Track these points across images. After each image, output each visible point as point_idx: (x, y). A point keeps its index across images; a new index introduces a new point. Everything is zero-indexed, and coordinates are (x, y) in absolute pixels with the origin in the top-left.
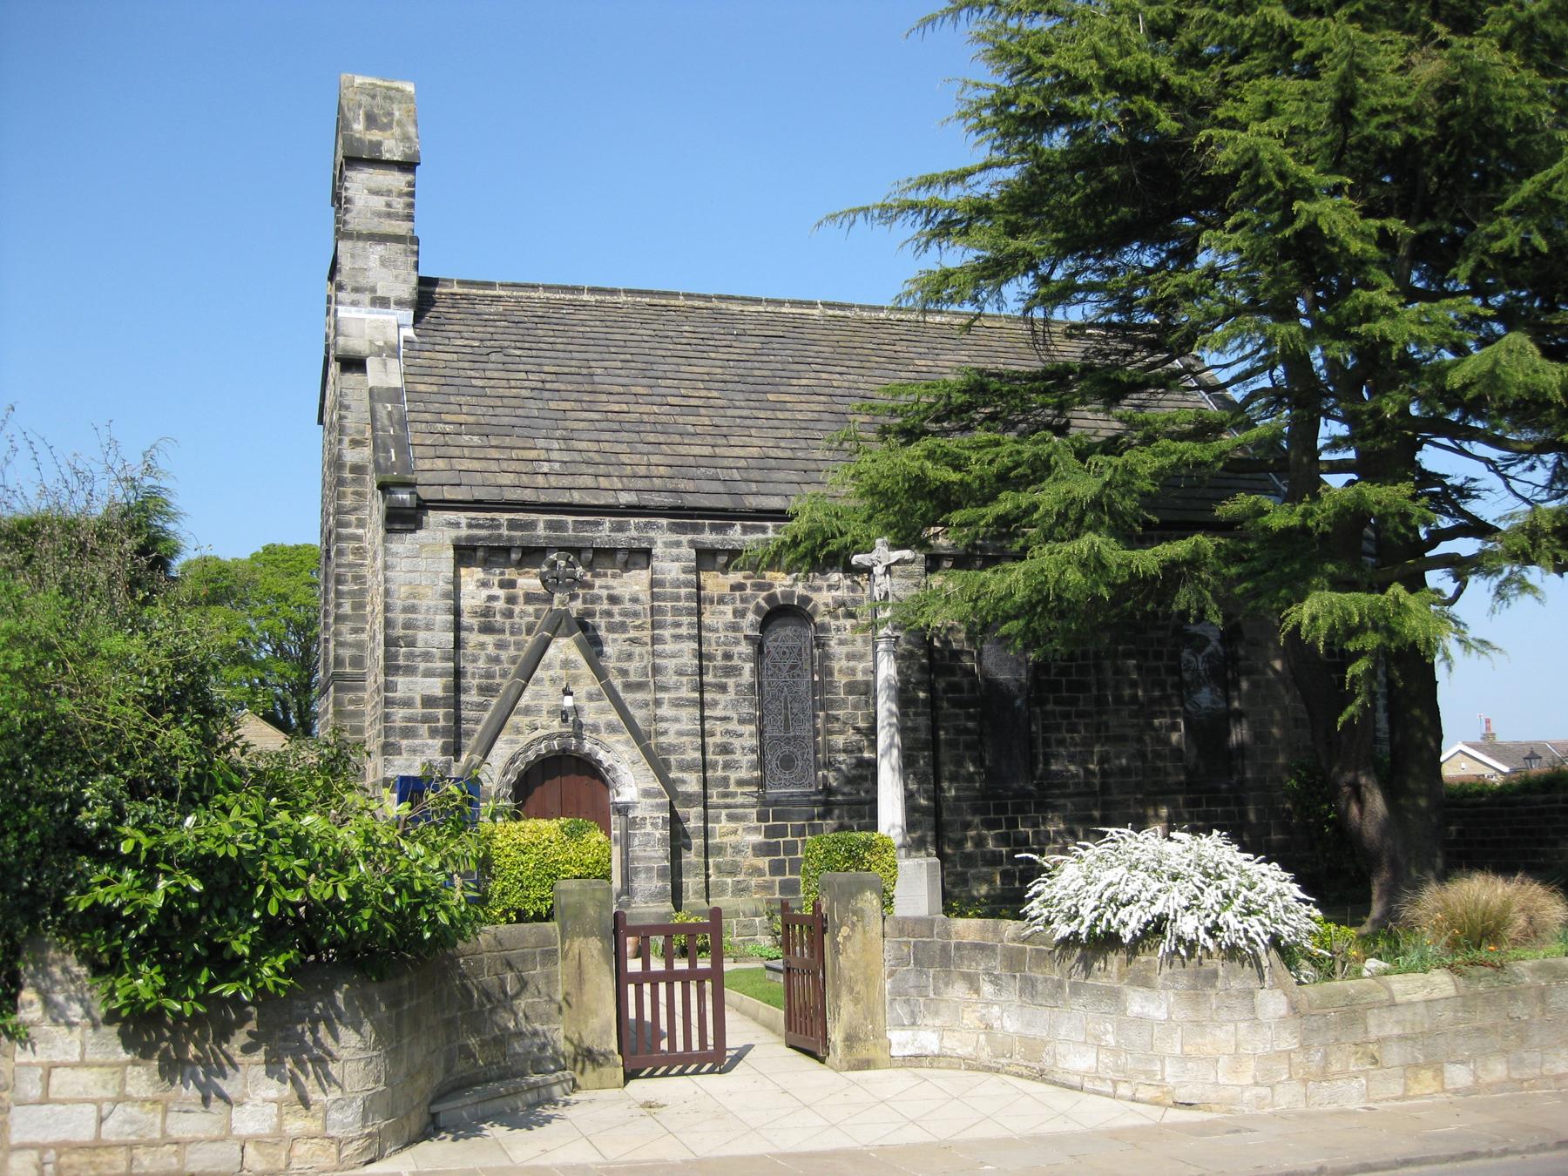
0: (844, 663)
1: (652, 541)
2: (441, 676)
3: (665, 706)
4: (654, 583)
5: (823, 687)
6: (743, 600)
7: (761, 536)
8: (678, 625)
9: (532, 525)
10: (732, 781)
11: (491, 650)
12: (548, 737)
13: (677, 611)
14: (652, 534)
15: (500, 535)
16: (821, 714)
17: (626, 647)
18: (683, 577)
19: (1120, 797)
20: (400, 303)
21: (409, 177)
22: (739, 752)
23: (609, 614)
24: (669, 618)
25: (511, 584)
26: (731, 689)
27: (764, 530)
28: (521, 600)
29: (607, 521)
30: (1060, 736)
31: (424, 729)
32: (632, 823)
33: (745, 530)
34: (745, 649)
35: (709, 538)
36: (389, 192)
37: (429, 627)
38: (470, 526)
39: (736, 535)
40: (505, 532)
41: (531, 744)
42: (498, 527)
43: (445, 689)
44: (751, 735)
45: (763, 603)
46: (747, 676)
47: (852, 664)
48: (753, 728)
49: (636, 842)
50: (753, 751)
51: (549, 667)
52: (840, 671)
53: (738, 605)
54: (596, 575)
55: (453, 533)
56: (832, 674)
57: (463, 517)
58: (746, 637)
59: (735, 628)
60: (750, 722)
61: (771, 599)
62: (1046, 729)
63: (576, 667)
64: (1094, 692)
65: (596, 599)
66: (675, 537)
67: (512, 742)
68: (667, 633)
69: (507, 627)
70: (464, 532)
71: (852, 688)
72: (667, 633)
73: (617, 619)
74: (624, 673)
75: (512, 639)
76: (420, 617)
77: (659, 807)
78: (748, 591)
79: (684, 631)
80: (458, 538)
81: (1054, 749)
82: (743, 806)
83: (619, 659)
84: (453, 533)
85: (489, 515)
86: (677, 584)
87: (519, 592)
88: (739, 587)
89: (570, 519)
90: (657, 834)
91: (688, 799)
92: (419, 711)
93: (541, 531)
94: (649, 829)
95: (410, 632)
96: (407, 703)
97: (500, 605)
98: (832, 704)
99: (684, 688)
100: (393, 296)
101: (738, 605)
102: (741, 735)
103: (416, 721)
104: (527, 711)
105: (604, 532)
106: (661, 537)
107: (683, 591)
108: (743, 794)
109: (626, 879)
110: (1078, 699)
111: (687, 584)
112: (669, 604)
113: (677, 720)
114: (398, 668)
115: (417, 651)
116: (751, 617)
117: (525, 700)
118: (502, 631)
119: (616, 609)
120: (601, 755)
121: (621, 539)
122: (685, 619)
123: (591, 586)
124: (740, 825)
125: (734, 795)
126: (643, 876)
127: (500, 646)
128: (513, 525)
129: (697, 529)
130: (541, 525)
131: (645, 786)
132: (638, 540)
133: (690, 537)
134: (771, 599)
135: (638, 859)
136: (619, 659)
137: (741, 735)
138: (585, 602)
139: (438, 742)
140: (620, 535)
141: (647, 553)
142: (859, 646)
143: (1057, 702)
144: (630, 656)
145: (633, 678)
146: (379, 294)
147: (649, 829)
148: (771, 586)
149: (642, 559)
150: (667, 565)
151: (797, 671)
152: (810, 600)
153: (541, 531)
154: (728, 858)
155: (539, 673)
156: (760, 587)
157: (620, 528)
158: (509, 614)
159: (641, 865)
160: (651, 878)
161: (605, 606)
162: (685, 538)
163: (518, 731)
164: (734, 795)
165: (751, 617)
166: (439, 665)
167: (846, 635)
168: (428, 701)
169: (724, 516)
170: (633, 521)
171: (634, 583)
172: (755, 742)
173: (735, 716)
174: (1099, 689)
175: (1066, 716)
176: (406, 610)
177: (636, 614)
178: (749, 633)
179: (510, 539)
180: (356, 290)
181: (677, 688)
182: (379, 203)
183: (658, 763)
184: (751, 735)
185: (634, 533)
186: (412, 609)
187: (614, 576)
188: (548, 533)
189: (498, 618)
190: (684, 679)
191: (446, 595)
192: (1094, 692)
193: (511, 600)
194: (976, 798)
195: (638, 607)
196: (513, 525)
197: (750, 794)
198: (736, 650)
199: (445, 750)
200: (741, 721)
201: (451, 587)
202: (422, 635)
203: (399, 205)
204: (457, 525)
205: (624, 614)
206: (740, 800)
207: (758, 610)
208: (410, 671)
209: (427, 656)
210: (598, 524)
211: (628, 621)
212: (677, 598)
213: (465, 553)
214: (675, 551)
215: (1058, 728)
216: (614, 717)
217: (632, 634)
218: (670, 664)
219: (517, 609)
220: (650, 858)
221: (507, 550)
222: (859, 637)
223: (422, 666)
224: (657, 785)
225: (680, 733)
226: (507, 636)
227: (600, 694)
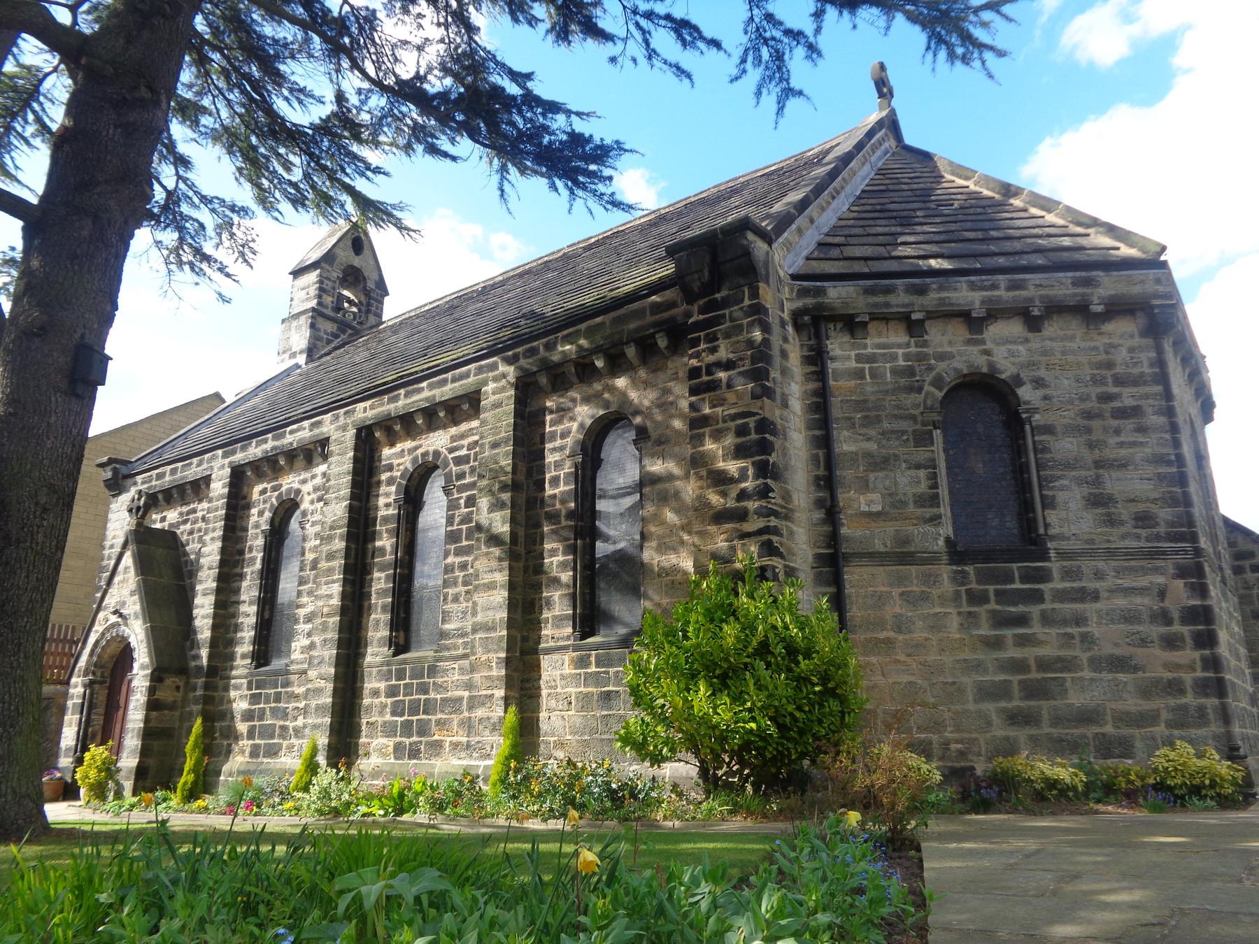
194: (382, 665)
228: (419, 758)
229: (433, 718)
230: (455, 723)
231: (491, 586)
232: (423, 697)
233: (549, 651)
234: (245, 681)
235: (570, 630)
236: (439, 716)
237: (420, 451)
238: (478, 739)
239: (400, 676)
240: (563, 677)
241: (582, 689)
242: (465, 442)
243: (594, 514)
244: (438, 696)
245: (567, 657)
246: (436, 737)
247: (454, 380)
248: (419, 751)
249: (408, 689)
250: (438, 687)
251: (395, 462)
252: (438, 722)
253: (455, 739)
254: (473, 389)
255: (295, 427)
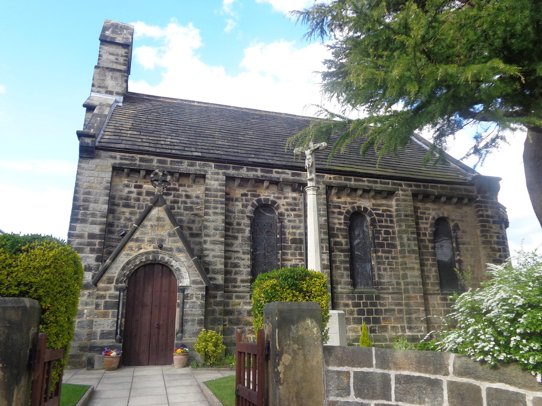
0: (291, 230)
1: (206, 172)
2: (99, 224)
3: (208, 244)
4: (207, 189)
5: (283, 240)
6: (246, 201)
7: (255, 173)
8: (216, 208)
9: (151, 161)
10: (239, 280)
11: (127, 215)
12: (147, 253)
13: (216, 202)
14: (206, 169)
15: (136, 164)
16: (280, 252)
17: (192, 218)
18: (219, 187)
19: (414, 295)
20: (118, 94)
21: (126, 50)
22: (242, 267)
23: (185, 203)
24: (212, 205)
25: (140, 187)
26: (240, 239)
27: (256, 171)
28: (144, 194)
29: (186, 162)
30: (385, 267)
31: (88, 249)
32: (185, 297)
33: (248, 170)
34: (247, 221)
35: (232, 172)
36: (117, 55)
37: (96, 202)
38: (121, 159)
39: (244, 172)
40: (138, 162)
41: (136, 257)
42: (135, 160)
43: (101, 230)
44: (248, 260)
45: (255, 203)
46: (247, 233)
47: (294, 230)
48: (249, 256)
49: (188, 306)
50: (249, 267)
51: (150, 220)
52: (289, 233)
53: (244, 202)
54: (180, 185)
55: (113, 161)
56: (285, 234)
57: (118, 155)
58: (248, 216)
59: (242, 212)
60: (248, 254)
61: (259, 201)
62: (378, 263)
63: (163, 221)
64: (399, 248)
65: (180, 196)
66: (217, 171)
67: (128, 254)
68: (211, 211)
69: (136, 205)
70: (118, 161)
71: (294, 241)
72: (211, 211)
73: (189, 205)
74: (190, 229)
75: (138, 211)
76: (92, 197)
77: (200, 289)
78: (249, 197)
79: (218, 211)
80: (115, 164)
81: (382, 272)
82: (243, 292)
83: (188, 223)
84: (113, 161)
85: (131, 155)
86: (217, 190)
87: (144, 191)
88: (246, 195)
89: (169, 160)
90: (198, 302)
91: (217, 287)
92: (86, 240)
93: (155, 163)
94: (194, 299)
95: (86, 203)
96: (81, 236)
97: (134, 195)
98: (285, 248)
99: (217, 236)
100: (115, 91)
101: (244, 202)
102: (244, 259)
103: (85, 245)
104: (137, 240)
105: (184, 166)
106: (211, 169)
107: (219, 194)
108: (243, 286)
109: (182, 325)
110: (392, 251)
111: (221, 191)
112: (212, 199)
113: (213, 250)
114: (78, 219)
115: (88, 212)
116: (250, 208)
117: (137, 235)
118: (134, 207)
119: (188, 201)
120: (173, 263)
121: (192, 170)
122: (219, 206)
123: (178, 190)
124: (242, 301)
125: (239, 287)
126: (190, 323)
127: (132, 213)
128: (141, 160)
129: (227, 168)
130: (155, 161)
131: (193, 279)
132: (200, 171)
133: (223, 171)
134: (259, 201)
135: (188, 315)
136: (188, 223)
137: (244, 259)
138: (174, 197)
139: (94, 256)
140: (191, 168)
141: (204, 177)
142: (297, 223)
143: (383, 252)
144: (193, 222)
145: (194, 231)
146: (109, 89)
147: (194, 299)
148: (259, 195)
149: (202, 181)
150: (213, 182)
151: (270, 233)
152: (276, 202)
153: (155, 163)
154: (235, 317)
155: (146, 223)
156: (254, 196)
157: (192, 165)
158: (138, 200)
159: (189, 318)
160: (193, 325)
161: (184, 199)
162: (221, 171)
163: (131, 249)
164: (239, 287)
165: (250, 208)
166: (99, 219)
167: (291, 218)
168: (92, 236)
169: (239, 164)
170: (198, 162)
171: (197, 191)
172: (249, 263)
173: (241, 251)
174: (401, 247)
175: (387, 258)
176: (85, 193)
177: (197, 204)
178: (249, 215)
179: (140, 165)
180: (99, 87)
181: (214, 236)
182: (113, 58)
183: (203, 266)
184: (248, 260)
185: (198, 168)
186: (89, 193)
187: (189, 186)
188: (158, 165)
189: (132, 201)
190: (218, 232)
191: (106, 188)
192: (399, 248)
193: (140, 194)
194: (349, 293)
195: (199, 201)
196: (141, 160)
197: (247, 287)
198: (243, 221)
199: (97, 259)
200: (244, 253)
201: (109, 185)
202: (92, 205)
203: (121, 60)
204: (115, 158)
205: (192, 203)
206: (241, 289)
207: (253, 205)
208: (84, 221)
209: (93, 215)
210: (181, 162)
211: (194, 206)
212: (216, 196)
213: (117, 170)
214: (216, 176)
215: (384, 263)
216: (180, 244)
217: (195, 212)
218: (211, 225)
219: (142, 198)
220: (194, 315)
221: (138, 171)
222: (297, 220)
223: (91, 219)
224: (200, 278)
225: (214, 256)
226: (136, 210)
227: (174, 234)
228: (376, 333)
229: (381, 317)
230: (392, 319)
231: (413, 269)
232: (374, 308)
233: (431, 294)
234: (249, 294)
235: (438, 288)
236: (384, 316)
237: (356, 205)
238: (415, 325)
239: (360, 298)
240: (438, 304)
241: (445, 308)
242: (381, 208)
243: (252, 246)
244: (383, 308)
245: (438, 297)
246: (383, 324)
247: (381, 183)
248: (375, 330)
249: (365, 305)
250: (382, 305)
251: (342, 206)
252: (384, 318)
253: (392, 325)
254: (392, 190)
255: (280, 170)
